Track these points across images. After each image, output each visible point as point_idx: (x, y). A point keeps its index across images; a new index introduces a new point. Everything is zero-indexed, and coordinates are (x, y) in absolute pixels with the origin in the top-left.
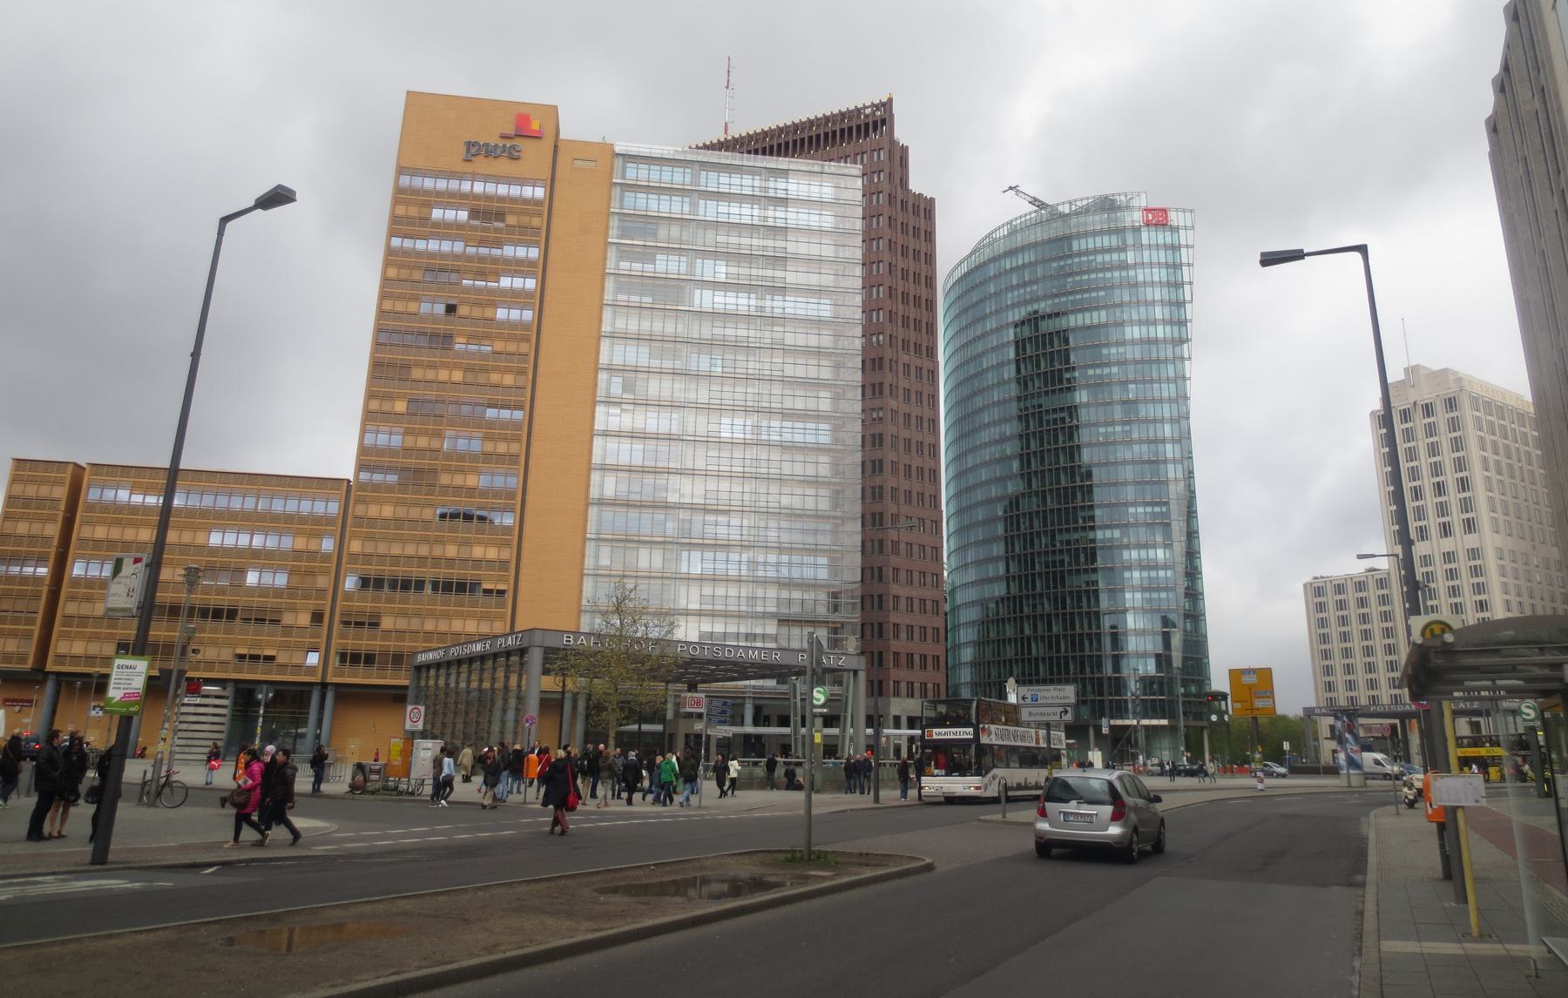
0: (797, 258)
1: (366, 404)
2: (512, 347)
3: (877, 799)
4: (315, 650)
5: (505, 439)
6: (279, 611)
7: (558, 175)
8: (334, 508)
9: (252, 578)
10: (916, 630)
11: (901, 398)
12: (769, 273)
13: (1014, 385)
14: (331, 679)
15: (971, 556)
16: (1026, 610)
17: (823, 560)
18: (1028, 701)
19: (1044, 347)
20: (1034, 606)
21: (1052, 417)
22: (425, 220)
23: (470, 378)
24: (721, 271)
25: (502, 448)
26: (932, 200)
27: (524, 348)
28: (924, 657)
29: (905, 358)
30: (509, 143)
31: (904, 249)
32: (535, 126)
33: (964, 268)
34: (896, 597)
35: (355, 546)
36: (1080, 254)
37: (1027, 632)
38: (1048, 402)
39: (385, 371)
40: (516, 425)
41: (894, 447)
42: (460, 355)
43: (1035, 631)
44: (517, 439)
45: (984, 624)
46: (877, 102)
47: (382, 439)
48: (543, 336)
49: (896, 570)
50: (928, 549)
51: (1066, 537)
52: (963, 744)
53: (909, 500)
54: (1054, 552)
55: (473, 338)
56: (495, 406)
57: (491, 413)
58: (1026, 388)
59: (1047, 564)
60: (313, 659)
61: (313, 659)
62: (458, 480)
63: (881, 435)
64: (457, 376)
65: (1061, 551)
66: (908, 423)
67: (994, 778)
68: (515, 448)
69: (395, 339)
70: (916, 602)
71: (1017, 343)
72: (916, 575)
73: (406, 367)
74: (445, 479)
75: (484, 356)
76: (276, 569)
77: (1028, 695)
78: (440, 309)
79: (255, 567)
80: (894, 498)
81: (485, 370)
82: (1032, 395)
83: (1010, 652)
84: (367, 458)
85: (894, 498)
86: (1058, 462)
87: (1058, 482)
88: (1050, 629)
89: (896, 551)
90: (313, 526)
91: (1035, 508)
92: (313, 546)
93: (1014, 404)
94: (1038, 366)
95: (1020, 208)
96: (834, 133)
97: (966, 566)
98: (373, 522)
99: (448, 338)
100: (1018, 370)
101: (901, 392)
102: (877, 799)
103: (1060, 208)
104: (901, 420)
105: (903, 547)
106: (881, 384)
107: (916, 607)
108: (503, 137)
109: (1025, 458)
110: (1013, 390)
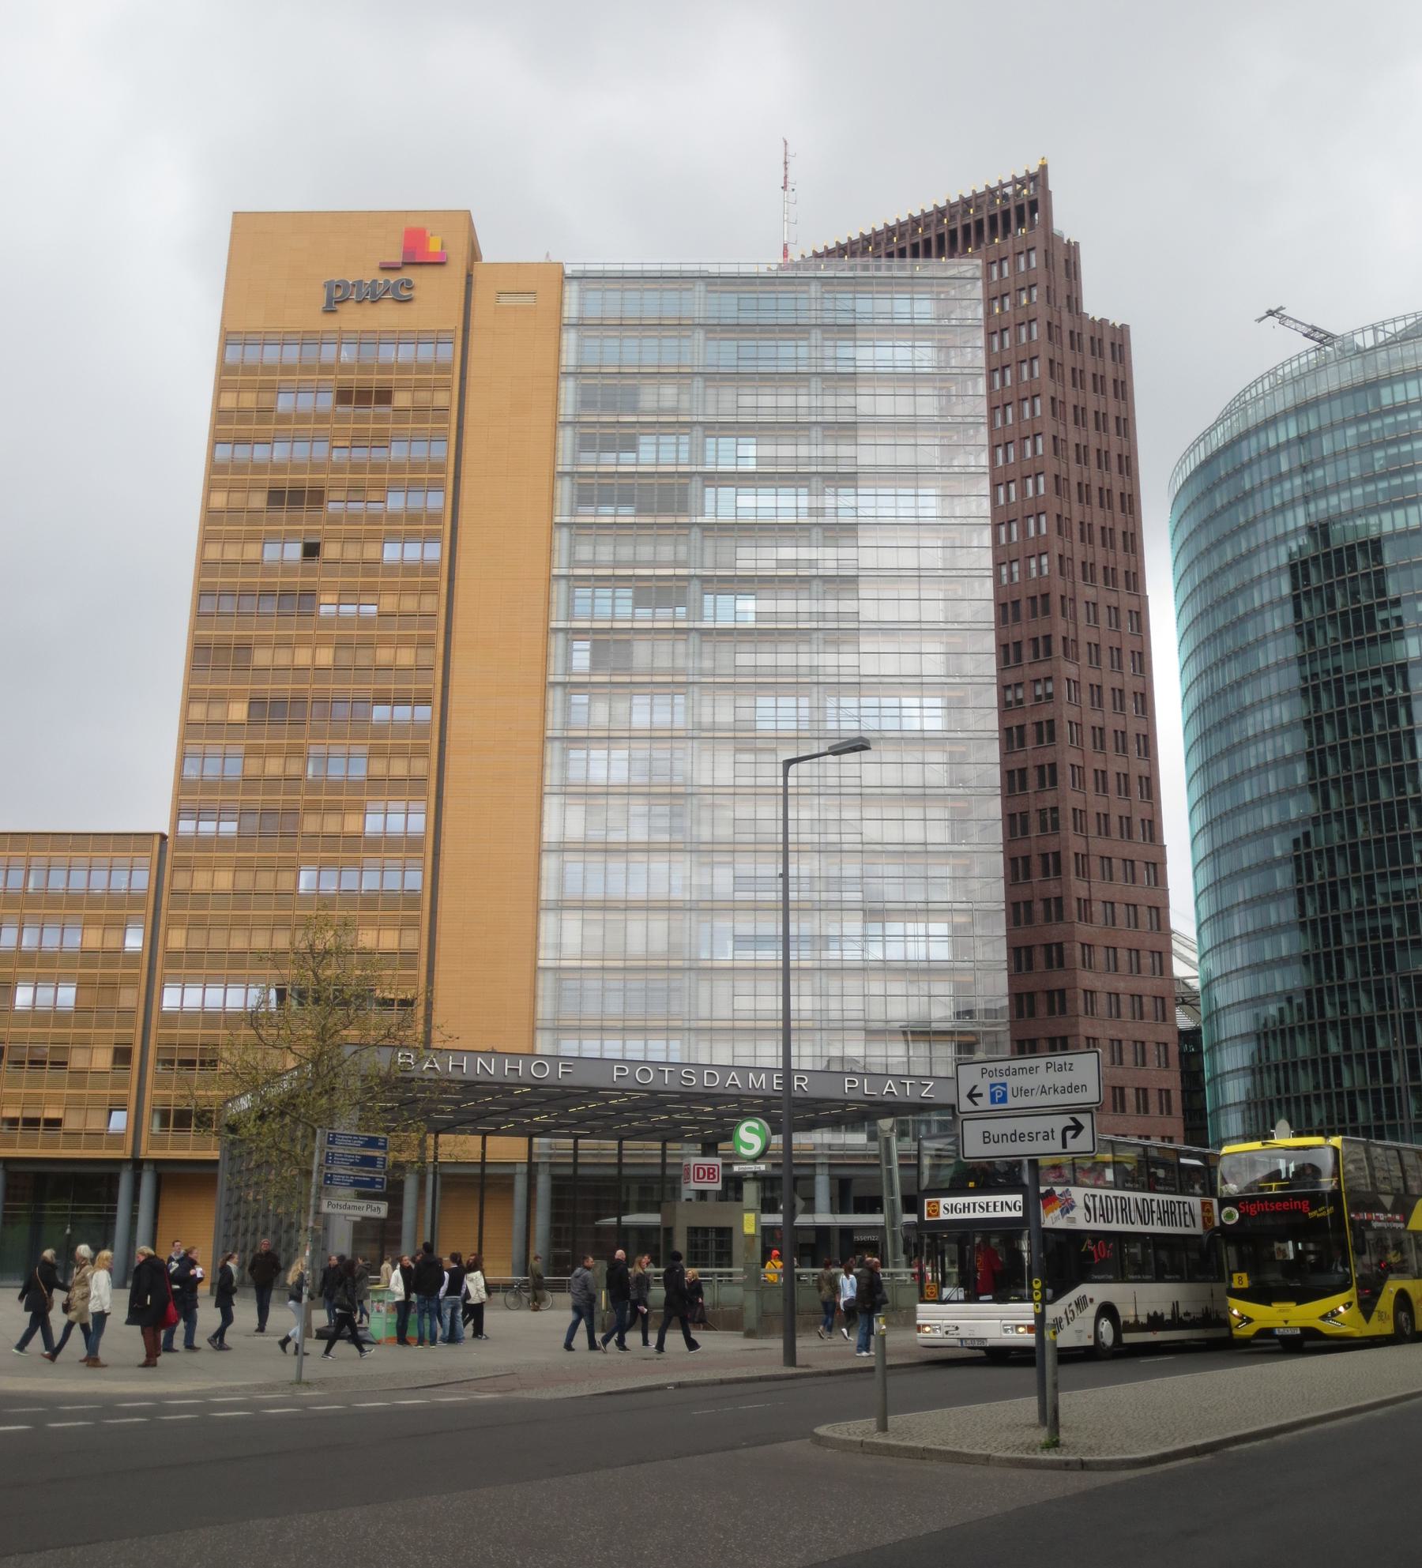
0: (877, 424)
1: (186, 711)
2: (409, 604)
3: (790, 1356)
4: (122, 1107)
5: (400, 752)
6: (63, 1047)
7: (476, 321)
8: (142, 880)
9: (23, 997)
10: (1128, 1048)
11: (1084, 659)
12: (829, 450)
13: (1292, 638)
14: (148, 1152)
15: (1238, 924)
16: (1329, 1012)
17: (940, 928)
18: (984, 1103)
19: (1341, 572)
20: (1344, 1005)
21: (1358, 686)
22: (265, 413)
23: (345, 657)
24: (748, 454)
25: (399, 768)
26: (1124, 330)
27: (429, 603)
28: (1142, 1092)
29: (1089, 593)
30: (393, 278)
31: (1079, 413)
32: (434, 246)
33: (1201, 454)
34: (1090, 993)
35: (176, 939)
36: (1395, 409)
37: (1334, 1047)
38: (1349, 662)
39: (211, 657)
40: (422, 730)
41: (1077, 742)
42: (328, 623)
43: (1347, 1046)
44: (423, 752)
45: (1263, 1036)
46: (1020, 174)
47: (213, 768)
48: (459, 583)
49: (1087, 947)
50: (1143, 911)
51: (1392, 886)
52: (1008, 1230)
53: (1104, 829)
54: (1372, 913)
55: (346, 594)
56: (385, 701)
57: (380, 713)
58: (1312, 640)
59: (1361, 933)
60: (119, 1121)
61: (119, 1121)
62: (332, 824)
63: (1051, 722)
64: (325, 657)
65: (1385, 911)
66: (1097, 702)
67: (1081, 1303)
68: (420, 767)
69: (228, 605)
70: (1125, 1000)
71: (1293, 568)
72: (1123, 955)
73: (244, 648)
74: (311, 824)
75: (365, 622)
76: (56, 981)
77: (984, 1088)
78: (294, 551)
79: (27, 978)
80: (1079, 827)
81: (369, 644)
82: (1324, 654)
83: (1305, 1083)
84: (191, 797)
85: (1079, 827)
86: (1372, 762)
87: (1375, 794)
88: (1372, 1042)
89: (1086, 915)
90: (112, 910)
91: (1337, 841)
92: (112, 942)
93: (1294, 670)
94: (1332, 603)
95: (1288, 348)
96: (953, 233)
97: (1230, 941)
98: (202, 898)
99: (309, 595)
100: (1298, 613)
101: (1083, 649)
102: (790, 1356)
103: (1358, 340)
104: (1086, 696)
105: (1097, 908)
106: (1048, 638)
107: (1126, 1009)
108: (386, 268)
109: (1315, 758)
110: (1291, 646)
